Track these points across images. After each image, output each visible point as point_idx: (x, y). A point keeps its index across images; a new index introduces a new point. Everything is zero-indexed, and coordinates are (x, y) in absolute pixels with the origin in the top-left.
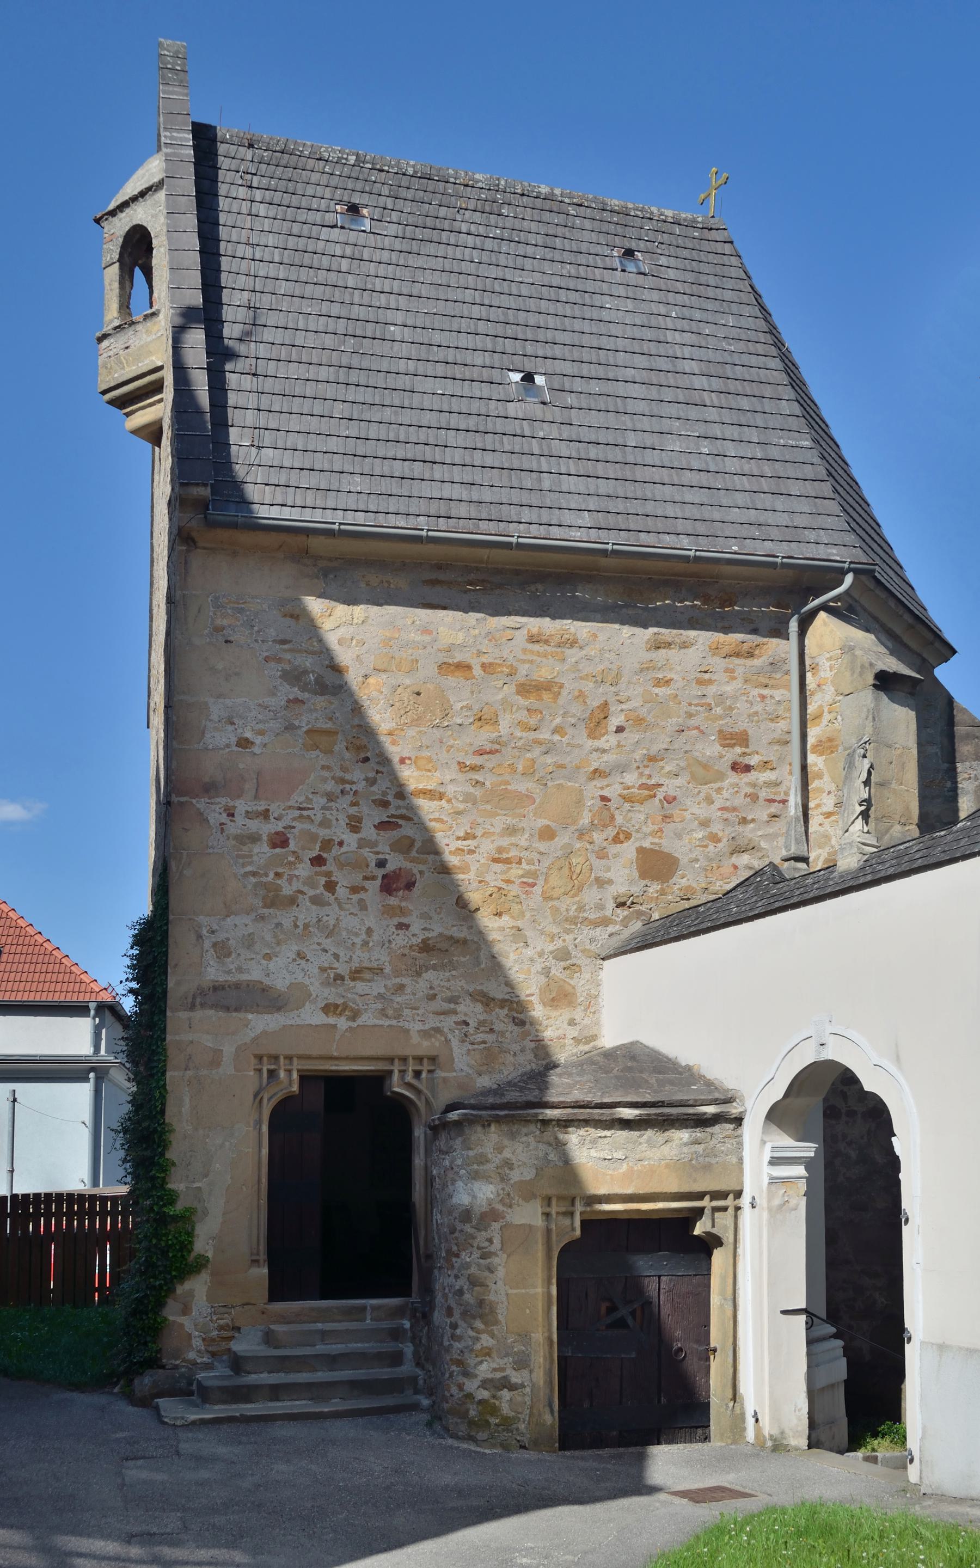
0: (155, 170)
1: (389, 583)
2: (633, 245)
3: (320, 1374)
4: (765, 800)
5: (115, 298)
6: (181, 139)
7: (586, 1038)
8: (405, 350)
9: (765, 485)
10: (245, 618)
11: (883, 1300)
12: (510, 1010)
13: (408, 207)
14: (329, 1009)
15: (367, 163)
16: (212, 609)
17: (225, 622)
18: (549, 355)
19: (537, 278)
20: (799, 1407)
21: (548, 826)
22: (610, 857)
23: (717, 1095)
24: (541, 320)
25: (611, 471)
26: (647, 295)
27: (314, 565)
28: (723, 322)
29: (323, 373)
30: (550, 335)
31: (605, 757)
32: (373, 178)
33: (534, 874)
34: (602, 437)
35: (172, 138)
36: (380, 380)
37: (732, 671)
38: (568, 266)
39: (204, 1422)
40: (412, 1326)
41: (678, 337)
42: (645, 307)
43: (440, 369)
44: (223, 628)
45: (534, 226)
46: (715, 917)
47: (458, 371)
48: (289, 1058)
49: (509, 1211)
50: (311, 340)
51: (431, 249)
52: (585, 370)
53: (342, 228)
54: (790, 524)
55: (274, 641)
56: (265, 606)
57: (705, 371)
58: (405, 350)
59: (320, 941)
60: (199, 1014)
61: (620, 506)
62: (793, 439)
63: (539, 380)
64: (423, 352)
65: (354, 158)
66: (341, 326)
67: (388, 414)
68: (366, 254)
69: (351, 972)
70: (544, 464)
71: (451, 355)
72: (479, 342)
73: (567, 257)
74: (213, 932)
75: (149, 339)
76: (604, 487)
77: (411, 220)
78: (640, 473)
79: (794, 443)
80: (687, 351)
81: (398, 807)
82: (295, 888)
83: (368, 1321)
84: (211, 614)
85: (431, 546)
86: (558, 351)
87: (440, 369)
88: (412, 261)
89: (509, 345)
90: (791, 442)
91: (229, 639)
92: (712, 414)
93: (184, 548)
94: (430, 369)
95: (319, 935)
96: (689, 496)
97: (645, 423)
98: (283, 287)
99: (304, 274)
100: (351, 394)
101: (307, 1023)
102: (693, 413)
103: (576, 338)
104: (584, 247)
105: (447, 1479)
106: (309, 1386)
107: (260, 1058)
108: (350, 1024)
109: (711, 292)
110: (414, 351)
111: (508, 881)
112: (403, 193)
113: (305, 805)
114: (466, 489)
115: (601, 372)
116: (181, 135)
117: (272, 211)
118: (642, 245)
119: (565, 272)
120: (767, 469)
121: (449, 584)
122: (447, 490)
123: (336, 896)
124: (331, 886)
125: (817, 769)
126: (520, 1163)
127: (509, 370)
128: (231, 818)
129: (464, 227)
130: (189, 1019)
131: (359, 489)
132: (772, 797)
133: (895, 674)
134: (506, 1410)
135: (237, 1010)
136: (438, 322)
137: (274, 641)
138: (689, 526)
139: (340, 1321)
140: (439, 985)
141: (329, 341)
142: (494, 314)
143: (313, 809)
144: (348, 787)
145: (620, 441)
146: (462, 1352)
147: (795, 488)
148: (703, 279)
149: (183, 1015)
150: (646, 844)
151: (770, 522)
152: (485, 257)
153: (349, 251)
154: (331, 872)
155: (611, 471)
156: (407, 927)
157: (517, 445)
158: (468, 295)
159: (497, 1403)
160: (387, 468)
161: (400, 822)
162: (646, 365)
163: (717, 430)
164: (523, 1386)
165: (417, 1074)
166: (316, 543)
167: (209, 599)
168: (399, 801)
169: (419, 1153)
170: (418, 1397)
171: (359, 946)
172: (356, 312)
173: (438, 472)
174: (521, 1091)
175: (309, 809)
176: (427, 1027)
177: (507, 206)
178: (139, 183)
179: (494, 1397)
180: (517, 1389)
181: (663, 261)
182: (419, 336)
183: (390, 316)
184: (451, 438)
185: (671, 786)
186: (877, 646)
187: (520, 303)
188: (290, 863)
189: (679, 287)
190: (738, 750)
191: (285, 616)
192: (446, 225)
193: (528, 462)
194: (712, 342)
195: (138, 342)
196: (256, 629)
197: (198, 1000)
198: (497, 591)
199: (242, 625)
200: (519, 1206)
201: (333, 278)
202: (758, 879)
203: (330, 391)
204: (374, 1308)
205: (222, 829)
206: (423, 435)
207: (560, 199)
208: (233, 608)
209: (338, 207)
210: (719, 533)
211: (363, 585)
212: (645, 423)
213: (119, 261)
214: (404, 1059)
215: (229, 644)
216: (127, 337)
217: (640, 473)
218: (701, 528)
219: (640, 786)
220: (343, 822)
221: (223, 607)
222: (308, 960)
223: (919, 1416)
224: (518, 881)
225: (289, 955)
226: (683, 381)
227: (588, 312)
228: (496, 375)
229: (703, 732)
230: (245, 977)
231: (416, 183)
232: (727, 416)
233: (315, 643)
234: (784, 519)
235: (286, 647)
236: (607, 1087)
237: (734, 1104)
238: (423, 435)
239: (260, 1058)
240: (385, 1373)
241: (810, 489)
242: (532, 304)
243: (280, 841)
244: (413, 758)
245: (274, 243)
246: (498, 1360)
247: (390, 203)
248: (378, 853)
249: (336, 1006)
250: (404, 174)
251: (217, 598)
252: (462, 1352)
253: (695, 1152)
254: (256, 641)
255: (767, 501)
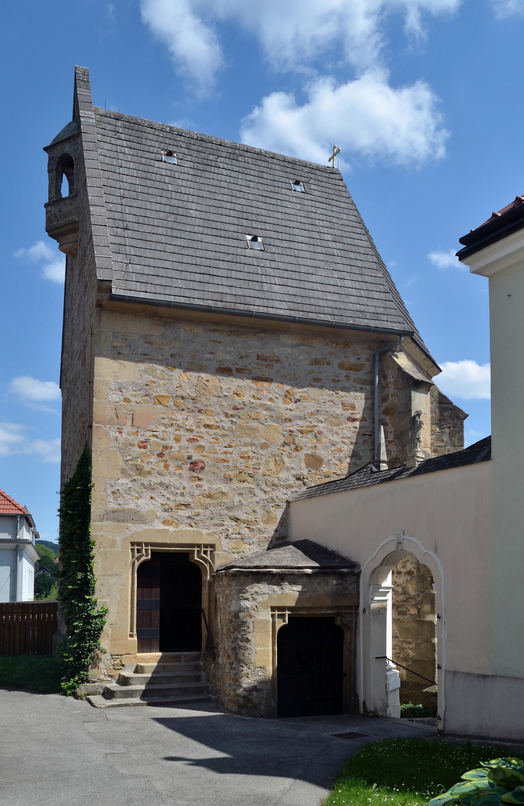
0: (74, 128)
1: (194, 329)
2: (299, 178)
3: (163, 685)
4: (362, 434)
5: (54, 187)
6: (89, 114)
7: (281, 537)
8: (198, 222)
9: (363, 293)
10: (127, 343)
11: (412, 653)
12: (248, 524)
13: (195, 154)
14: (164, 522)
15: (175, 131)
16: (112, 338)
17: (118, 344)
18: (264, 228)
19: (256, 191)
20: (383, 699)
21: (265, 443)
22: (293, 457)
23: (348, 564)
24: (259, 211)
25: (295, 283)
26: (306, 202)
27: (160, 320)
28: (341, 217)
29: (160, 231)
30: (263, 219)
31: (291, 413)
32: (178, 139)
33: (259, 464)
34: (289, 267)
35: (84, 114)
36: (186, 235)
37: (348, 376)
38: (270, 187)
39: (113, 706)
40: (204, 664)
41: (321, 223)
42: (305, 208)
43: (214, 232)
44: (117, 347)
45: (253, 167)
46: (346, 486)
47: (222, 233)
48: (147, 544)
49: (257, 613)
50: (154, 215)
51: (207, 174)
52: (280, 236)
53: (165, 162)
54: (375, 312)
55: (141, 354)
56: (137, 338)
57: (334, 240)
58: (198, 222)
59: (161, 492)
60: (105, 523)
61: (299, 300)
62: (374, 273)
63: (260, 239)
64: (206, 224)
65: (169, 128)
66: (168, 209)
67: (192, 252)
68: (177, 175)
69: (175, 506)
70: (264, 279)
71: (219, 225)
72: (231, 220)
73: (269, 182)
74: (112, 486)
75: (72, 208)
76: (292, 291)
77: (196, 160)
78: (307, 285)
79: (375, 275)
80: (325, 230)
81: (197, 432)
82: (150, 467)
83: (183, 662)
84: (111, 340)
85: (215, 314)
86: (267, 226)
87: (214, 232)
88: (198, 179)
89: (245, 223)
90: (373, 275)
91: (120, 352)
92: (338, 260)
93: (99, 309)
94: (209, 231)
95: (161, 489)
96: (329, 297)
97: (309, 263)
98: (139, 189)
99: (149, 183)
100: (174, 241)
101: (155, 528)
102: (330, 258)
103: (275, 221)
104: (277, 178)
105: (235, 730)
106: (160, 690)
107: (133, 544)
108: (175, 529)
109: (335, 203)
110: (201, 222)
111: (247, 467)
112: (193, 147)
113: (155, 430)
114: (229, 289)
115: (287, 237)
116: (88, 113)
117: (132, 152)
118: (303, 179)
119: (269, 189)
120: (364, 286)
121: (222, 331)
122: (221, 289)
123: (169, 471)
124: (166, 467)
125: (385, 421)
126: (262, 593)
127: (246, 234)
128: (120, 434)
129: (221, 165)
130: (101, 526)
131: (180, 286)
132: (365, 433)
133: (422, 381)
134: (255, 701)
135: (123, 521)
136: (212, 209)
137: (141, 354)
138: (330, 311)
139: (170, 662)
140: (216, 513)
141: (162, 215)
142: (237, 207)
143: (158, 431)
144: (175, 422)
145: (298, 270)
146: (235, 675)
147: (376, 295)
148: (331, 197)
149: (98, 523)
150: (309, 452)
151: (366, 310)
152: (232, 180)
153: (168, 173)
154: (167, 460)
155: (295, 283)
156: (202, 486)
157: (251, 269)
158: (225, 198)
159: (251, 697)
160: (192, 277)
161: (198, 438)
162: (307, 235)
163: (340, 267)
164: (262, 690)
165: (205, 552)
166: (162, 310)
167: (111, 333)
168: (198, 429)
169: (205, 587)
170: (210, 695)
171: (179, 494)
172: (174, 202)
173: (216, 280)
174: (260, 561)
175: (156, 431)
176: (210, 531)
177: (240, 156)
178: (66, 133)
179: (250, 694)
180: (260, 691)
181: (313, 187)
182: (204, 215)
183: (189, 205)
184: (221, 264)
185: (321, 426)
186: (413, 368)
187: (248, 203)
188: (148, 456)
189: (320, 199)
190: (351, 411)
191: (146, 343)
192: (213, 163)
193: (255, 277)
194: (336, 226)
195: (66, 209)
196: (132, 348)
197: (105, 516)
198: (244, 336)
199: (126, 346)
200: (261, 611)
201: (163, 186)
202: (365, 470)
203: (163, 239)
204: (185, 656)
205: (116, 439)
206: (208, 262)
207: (264, 155)
208: (122, 338)
209: (162, 152)
210: (344, 315)
211: (182, 330)
212: (309, 263)
213: (56, 169)
214: (199, 546)
215: (120, 354)
216: (60, 206)
217: (307, 285)
218: (336, 312)
219: (307, 426)
220: (172, 437)
221: (117, 337)
222: (156, 500)
223: (443, 702)
224: (251, 467)
225: (147, 497)
226: (324, 243)
227: (281, 209)
228: (240, 236)
229: (334, 403)
230: (126, 507)
231: (199, 143)
232: (345, 261)
233: (160, 356)
234: (372, 310)
235: (147, 357)
236: (298, 560)
237: (356, 568)
238: (208, 262)
239: (133, 544)
240: (194, 685)
241: (382, 296)
242: (254, 203)
243: (143, 445)
244: (204, 410)
245: (133, 167)
246: (251, 679)
247: (186, 151)
248: (188, 452)
249: (169, 521)
250: (192, 138)
251: (114, 333)
252: (235, 675)
253: (339, 589)
254: (132, 354)
255: (364, 301)
